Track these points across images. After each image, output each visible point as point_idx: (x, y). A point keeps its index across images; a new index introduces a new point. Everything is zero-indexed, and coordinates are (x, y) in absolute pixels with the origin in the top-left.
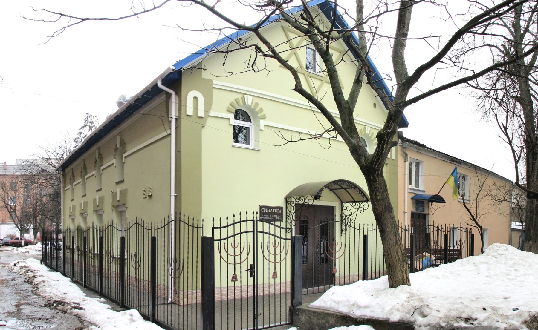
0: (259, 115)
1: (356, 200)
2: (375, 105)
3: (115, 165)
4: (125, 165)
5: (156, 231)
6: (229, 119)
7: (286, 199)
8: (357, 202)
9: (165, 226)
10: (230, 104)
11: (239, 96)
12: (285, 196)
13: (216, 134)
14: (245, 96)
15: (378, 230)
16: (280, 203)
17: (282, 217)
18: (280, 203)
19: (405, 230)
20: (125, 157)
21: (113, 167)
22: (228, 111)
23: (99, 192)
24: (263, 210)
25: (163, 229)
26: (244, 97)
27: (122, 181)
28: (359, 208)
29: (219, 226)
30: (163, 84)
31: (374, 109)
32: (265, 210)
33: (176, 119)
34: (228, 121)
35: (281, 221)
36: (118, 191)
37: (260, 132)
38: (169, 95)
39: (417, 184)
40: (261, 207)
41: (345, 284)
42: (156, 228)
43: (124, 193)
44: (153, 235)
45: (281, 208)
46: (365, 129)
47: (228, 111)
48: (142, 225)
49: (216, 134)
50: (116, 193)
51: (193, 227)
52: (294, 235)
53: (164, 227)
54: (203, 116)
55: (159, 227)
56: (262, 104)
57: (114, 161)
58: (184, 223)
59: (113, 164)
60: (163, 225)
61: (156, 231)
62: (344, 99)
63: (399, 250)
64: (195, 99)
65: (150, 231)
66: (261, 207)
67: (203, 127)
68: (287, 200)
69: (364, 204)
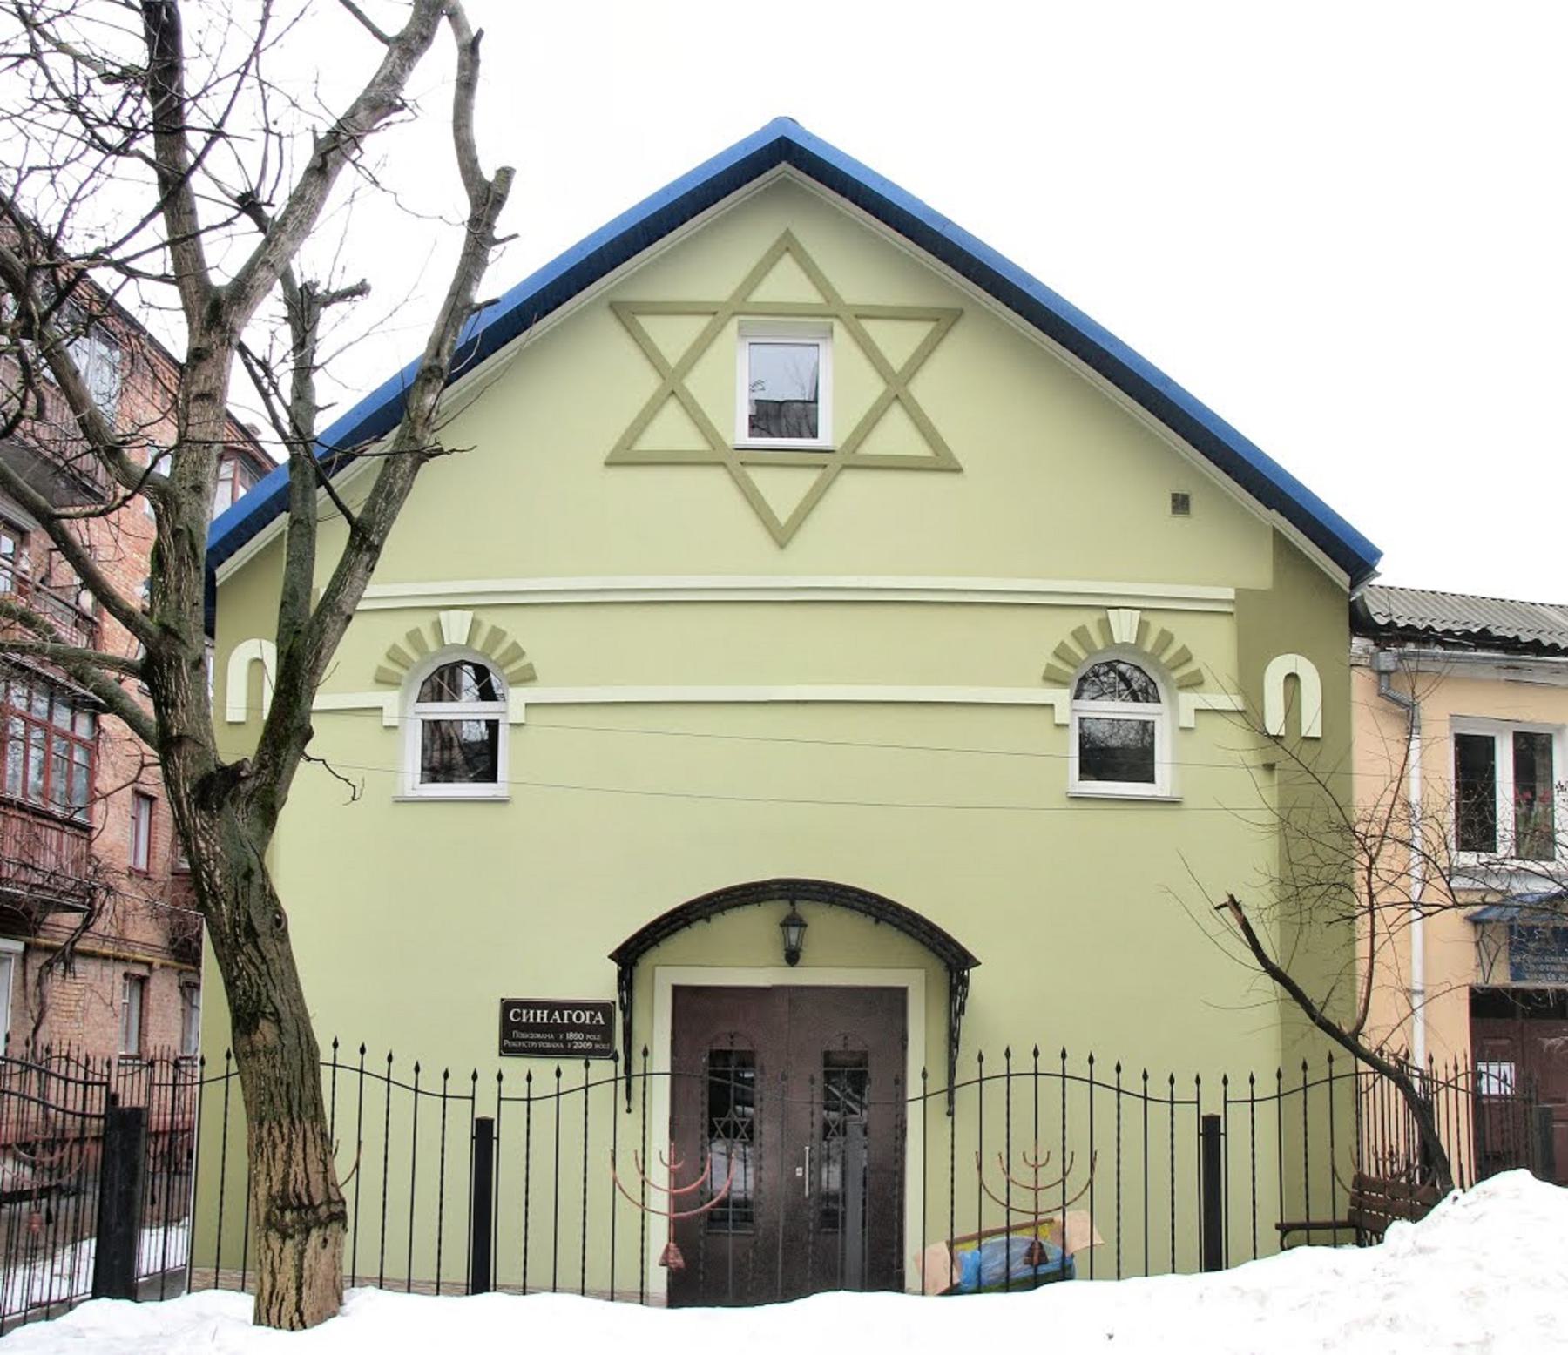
2: (1181, 504)
6: (1052, 706)
10: (1057, 654)
11: (1090, 620)
14: (443, 615)
15: (235, 1082)
18: (601, 984)
22: (384, 680)
31: (1180, 519)
32: (527, 1016)
39: (1537, 836)
40: (507, 1006)
41: (978, 1291)
46: (1105, 626)
47: (378, 681)
54: (242, 719)
56: (517, 628)
62: (779, 524)
63: (262, 1177)
66: (507, 1006)
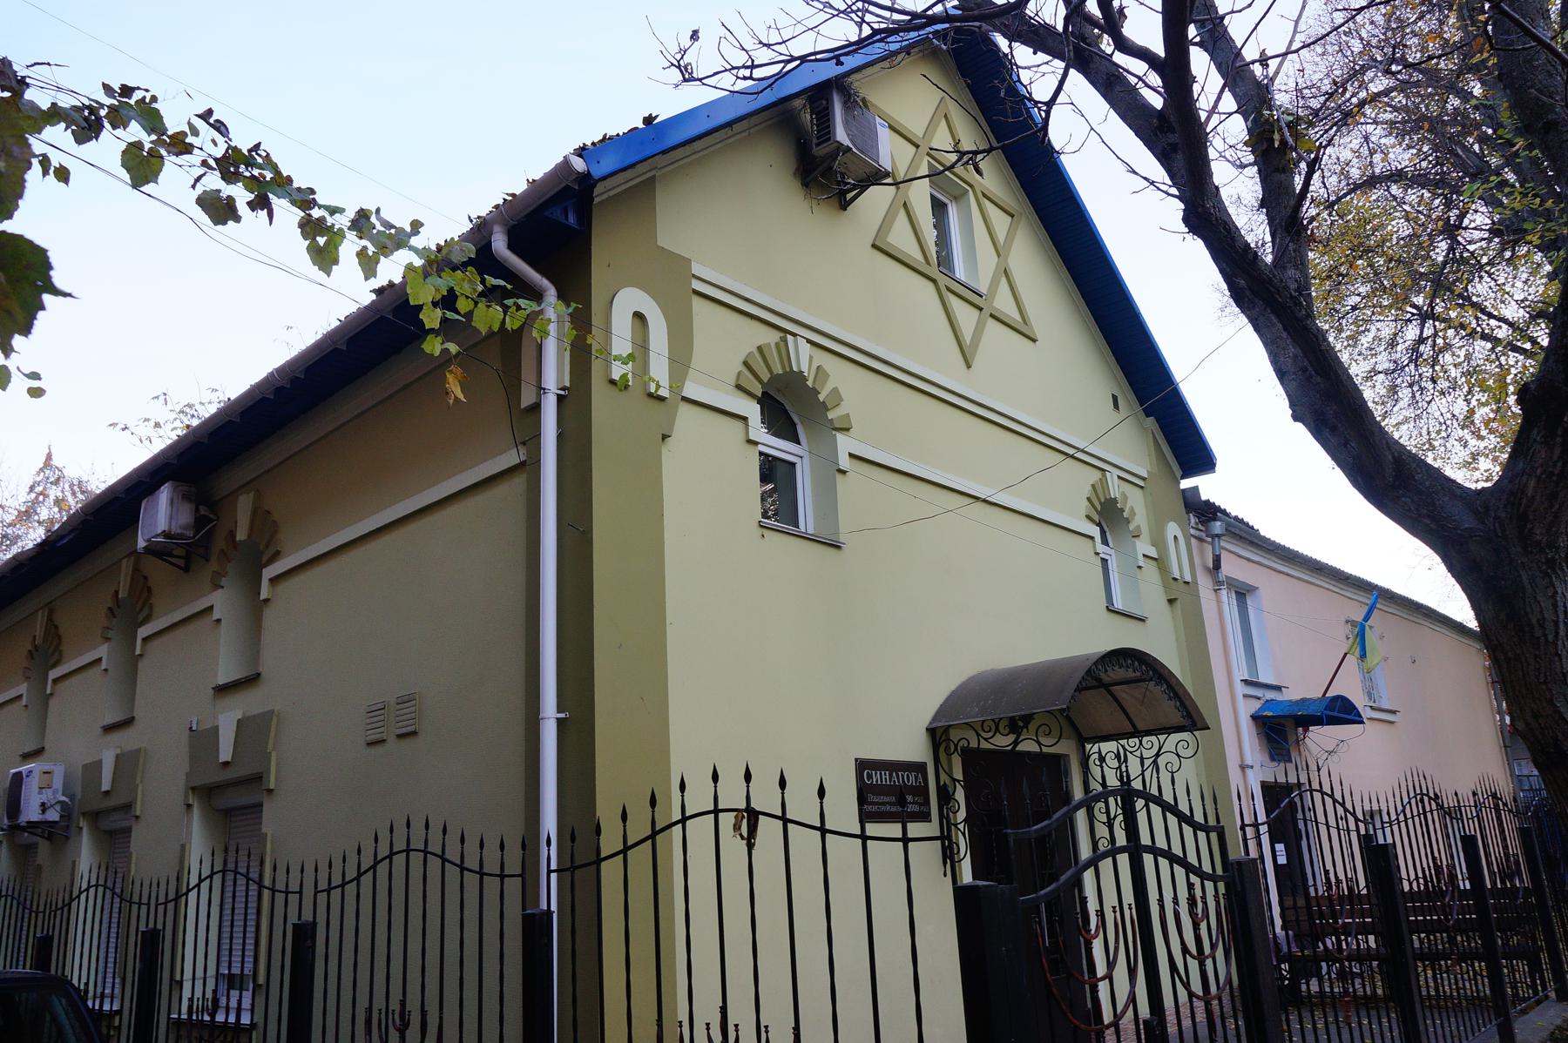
0: (831, 415)
1: (1141, 726)
3: (216, 616)
4: (269, 614)
5: (322, 897)
7: (931, 731)
8: (1149, 733)
9: (360, 875)
11: (772, 337)
12: (925, 718)
13: (706, 468)
16: (914, 748)
17: (927, 802)
18: (914, 748)
19: (140, 904)
20: (274, 581)
21: (206, 622)
23: (116, 737)
24: (870, 776)
25: (351, 889)
26: (785, 341)
27: (128, 722)
28: (1158, 755)
29: (910, 835)
30: (511, 247)
32: (877, 778)
33: (560, 398)
34: (739, 424)
35: (924, 817)
36: (227, 722)
37: (839, 476)
38: (537, 295)
40: (863, 766)
42: (323, 885)
43: (253, 731)
44: (307, 916)
45: (920, 768)
48: (1327, 789)
49: (706, 468)
50: (215, 731)
51: (482, 874)
52: (967, 877)
53: (357, 879)
55: (336, 881)
57: (102, 651)
58: (444, 860)
59: (20, 696)
60: (351, 873)
61: (322, 897)
64: (637, 321)
65: (144, 908)
67: (665, 437)
68: (938, 735)
69: (1175, 737)
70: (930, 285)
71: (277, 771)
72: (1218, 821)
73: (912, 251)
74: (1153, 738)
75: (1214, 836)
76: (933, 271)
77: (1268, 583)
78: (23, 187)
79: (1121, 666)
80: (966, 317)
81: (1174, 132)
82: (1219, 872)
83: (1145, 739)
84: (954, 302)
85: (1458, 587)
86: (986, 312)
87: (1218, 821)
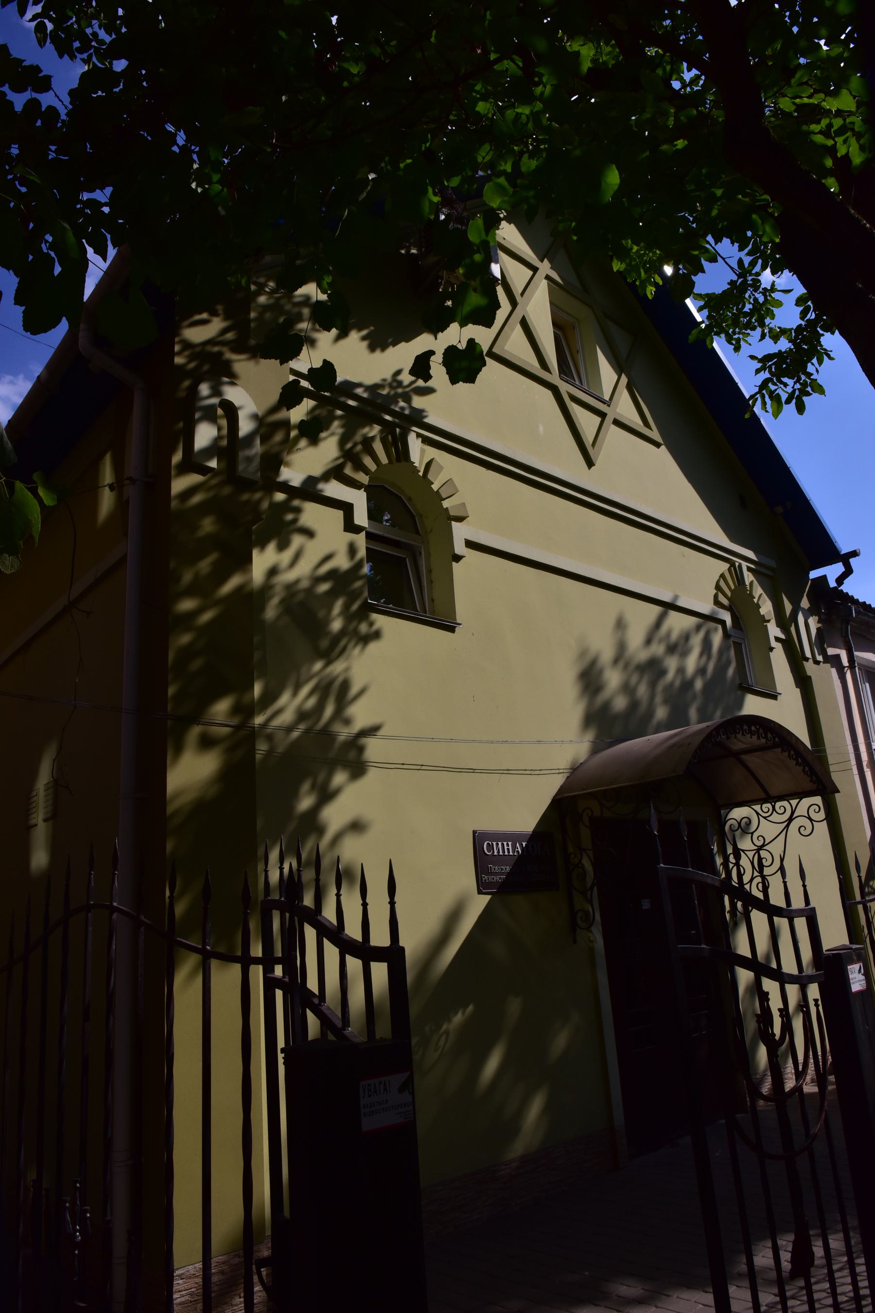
1: (773, 793)
8: (781, 798)
70: (548, 393)
71: (584, 789)
72: (807, 901)
73: (531, 361)
74: (785, 803)
75: (801, 924)
76: (554, 378)
77: (199, 981)
78: (16, 92)
79: (752, 733)
80: (587, 422)
81: (105, 260)
82: (809, 971)
83: (778, 804)
84: (577, 411)
85: (201, 1064)
86: (609, 419)
87: (807, 901)
